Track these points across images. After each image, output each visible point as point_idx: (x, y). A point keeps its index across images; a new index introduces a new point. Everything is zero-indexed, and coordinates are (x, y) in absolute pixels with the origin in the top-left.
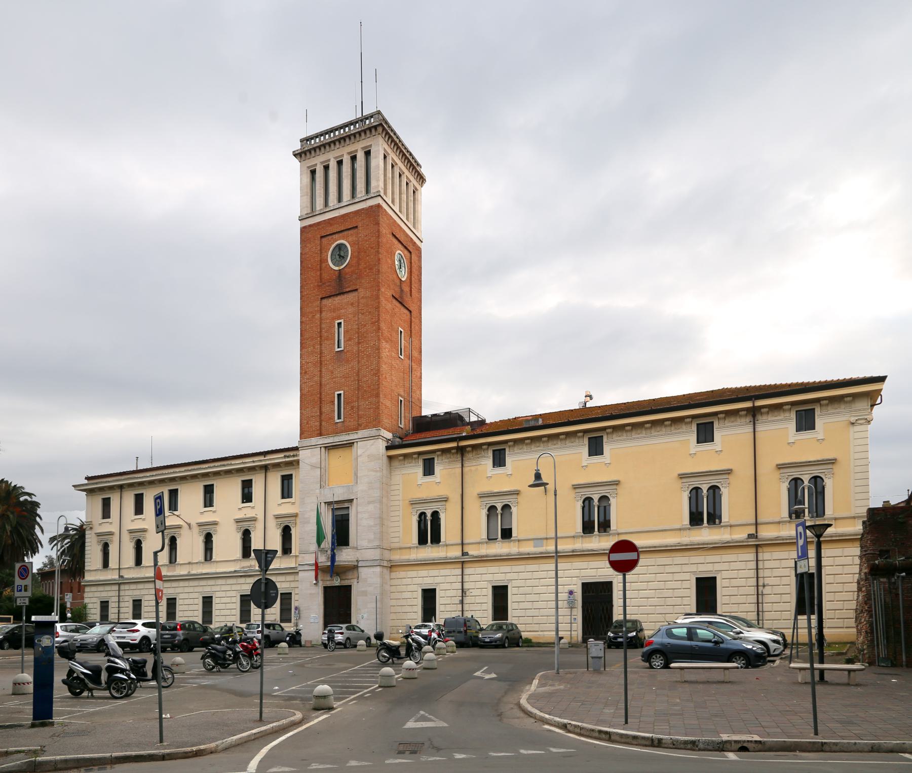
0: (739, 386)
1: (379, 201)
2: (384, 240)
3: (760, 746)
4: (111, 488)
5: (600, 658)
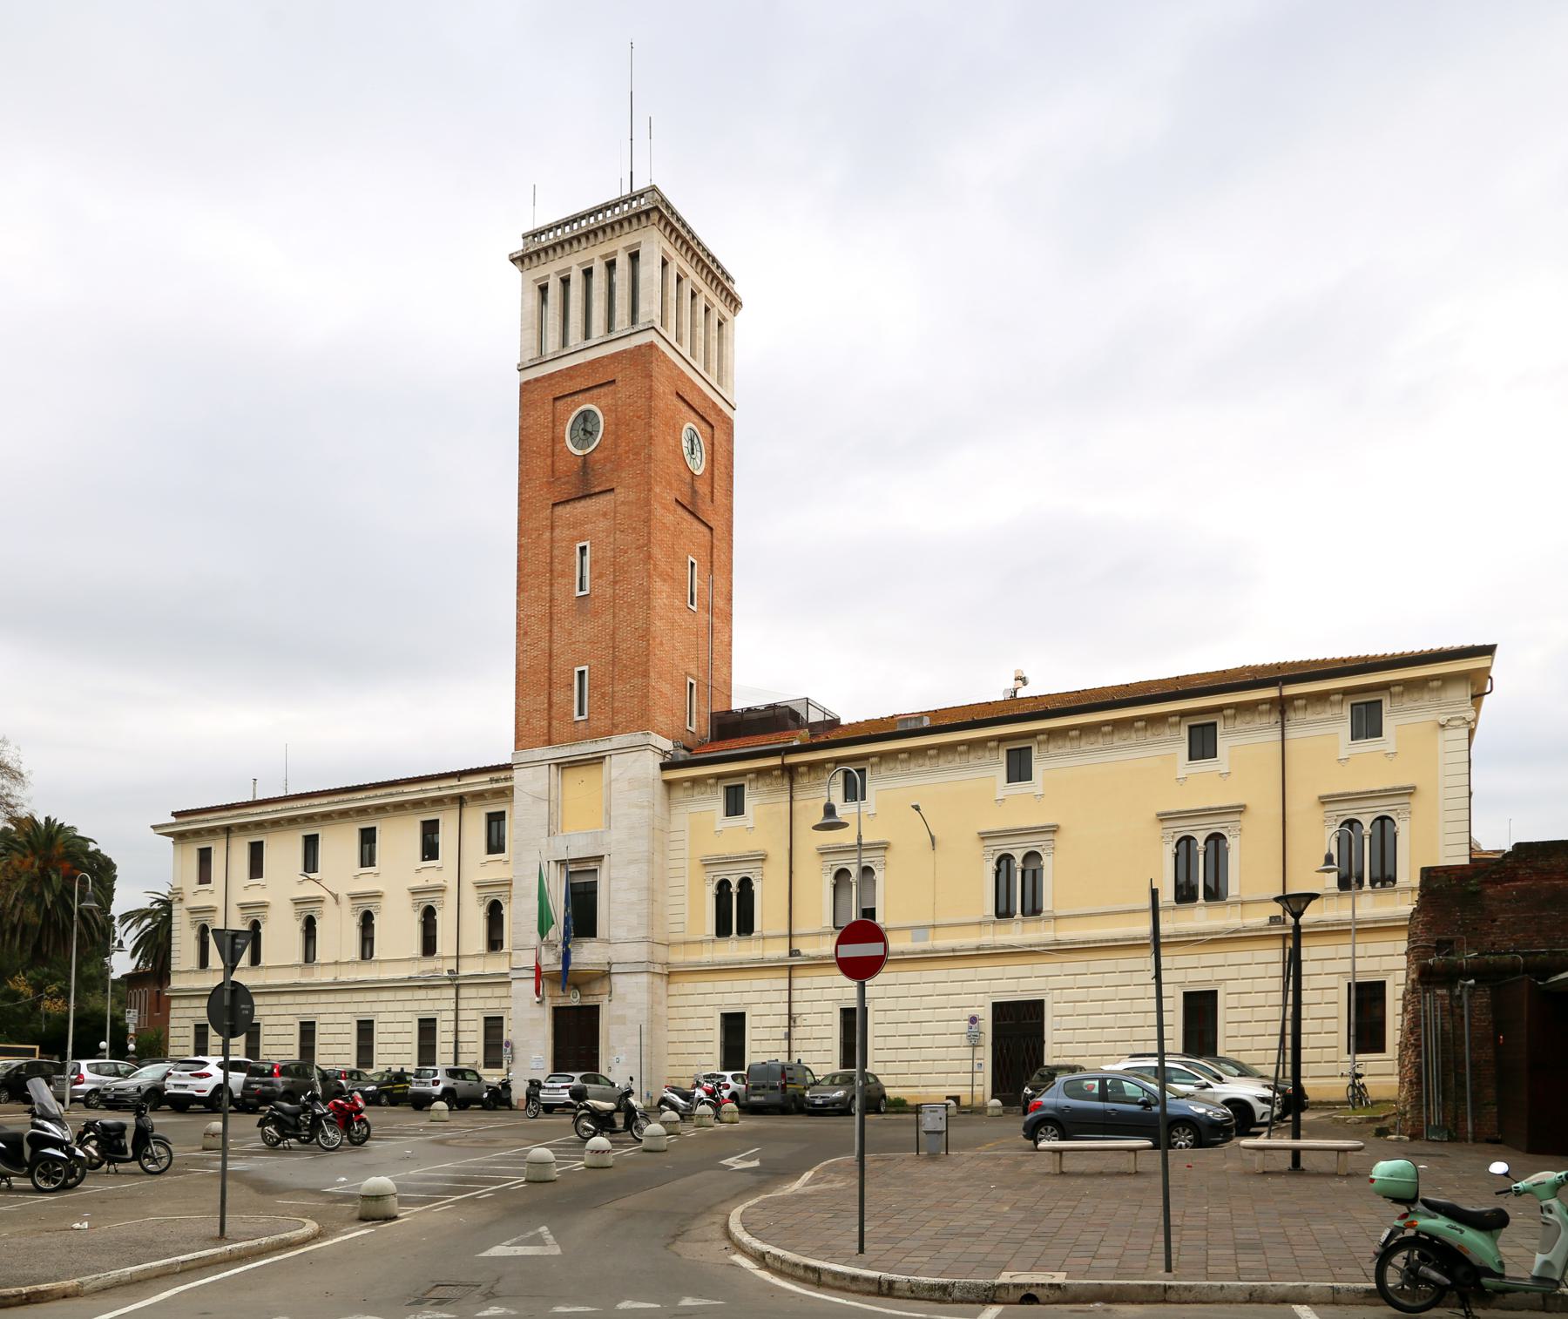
0: (1268, 663)
1: (651, 337)
2: (661, 405)
3: (1058, 1293)
4: (212, 831)
5: (940, 1133)
